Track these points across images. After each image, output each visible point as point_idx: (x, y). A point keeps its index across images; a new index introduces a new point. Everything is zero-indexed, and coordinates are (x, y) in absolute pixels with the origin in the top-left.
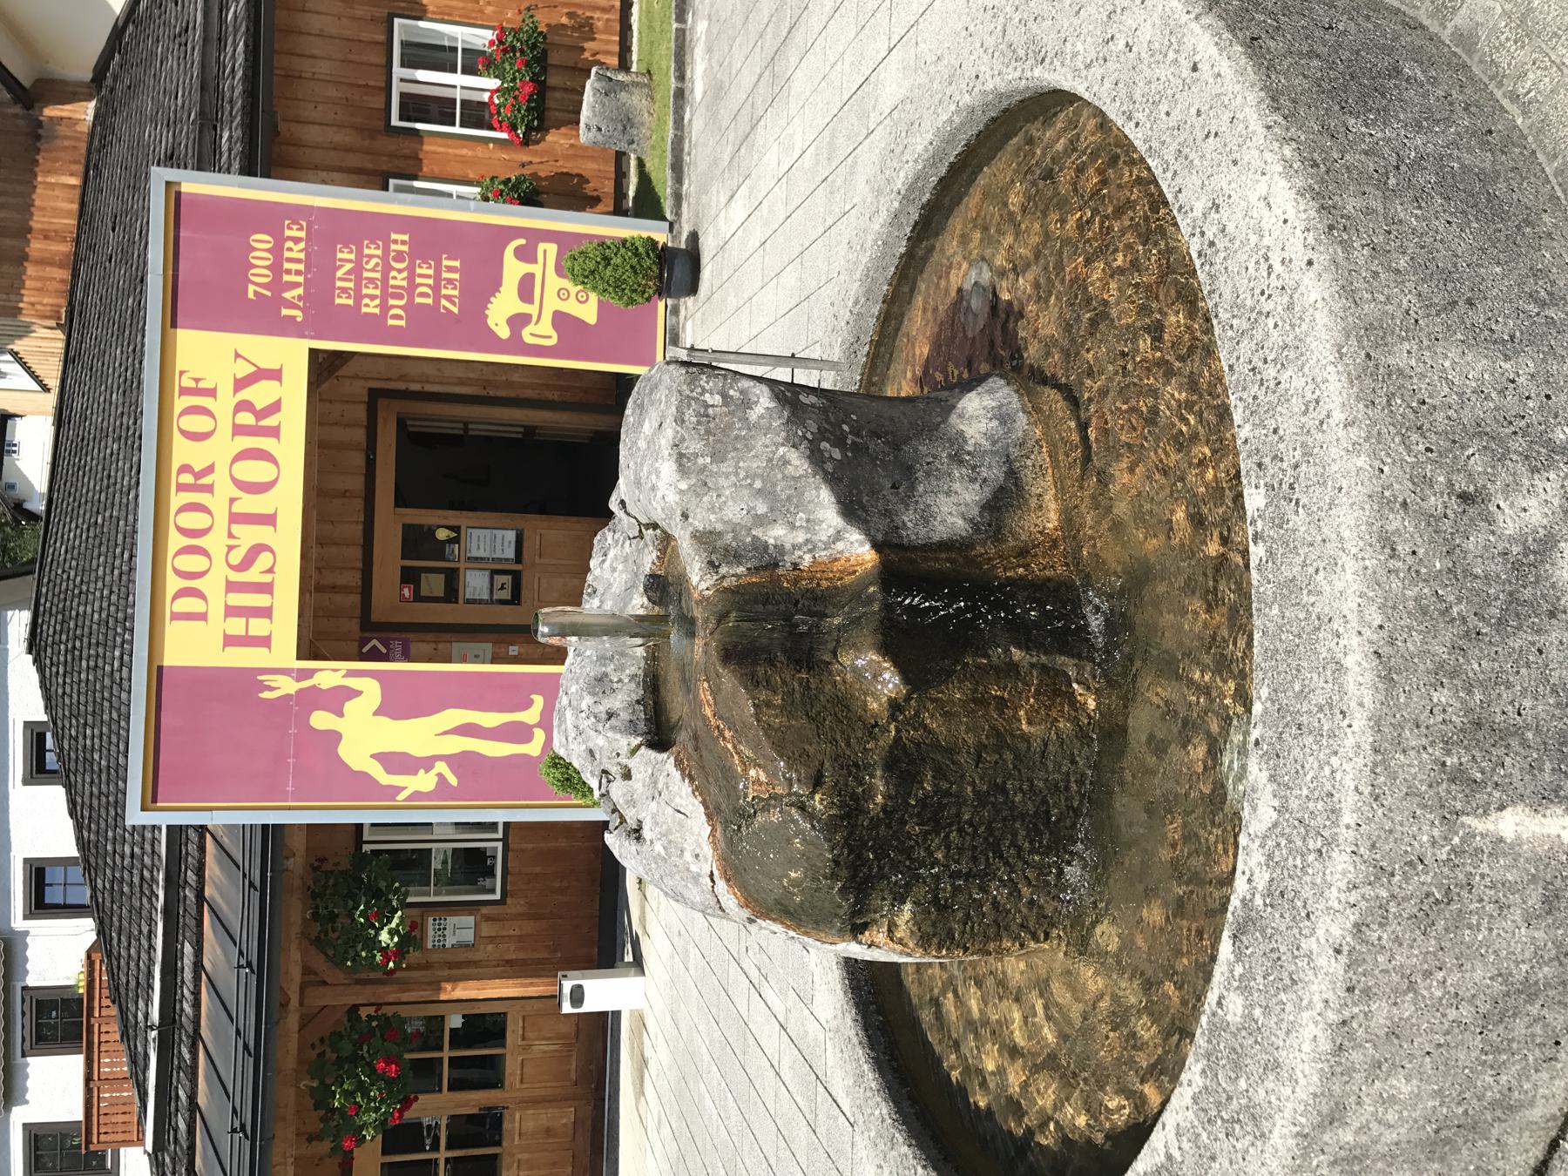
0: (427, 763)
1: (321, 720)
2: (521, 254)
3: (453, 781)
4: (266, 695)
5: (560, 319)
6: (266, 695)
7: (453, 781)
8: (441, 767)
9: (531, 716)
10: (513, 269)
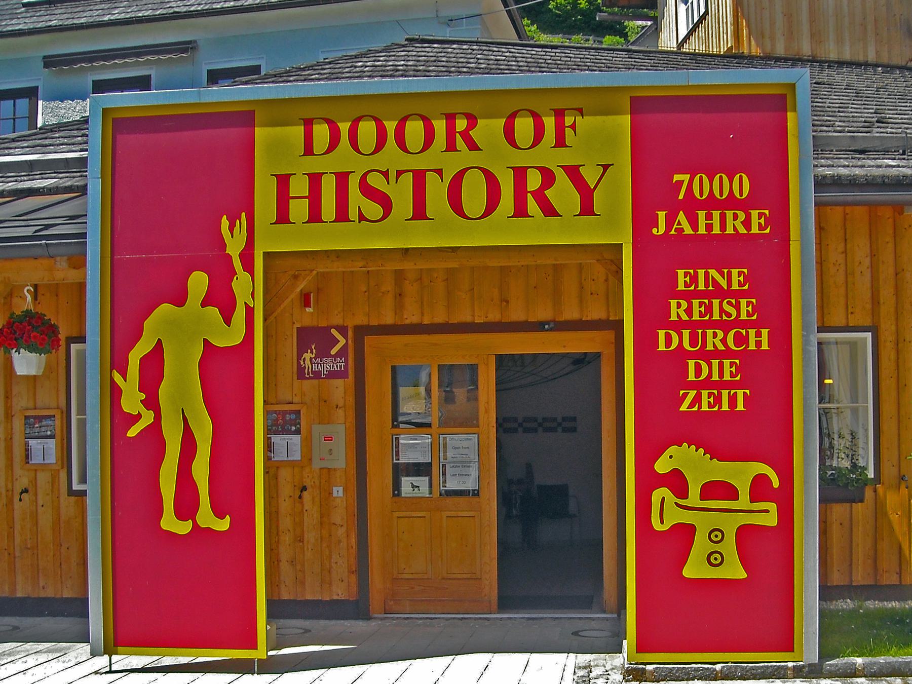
0: (151, 403)
1: (198, 282)
2: (760, 482)
3: (132, 432)
4: (225, 222)
5: (685, 532)
6: (225, 222)
7: (132, 432)
8: (148, 418)
9: (206, 517)
10: (742, 474)
